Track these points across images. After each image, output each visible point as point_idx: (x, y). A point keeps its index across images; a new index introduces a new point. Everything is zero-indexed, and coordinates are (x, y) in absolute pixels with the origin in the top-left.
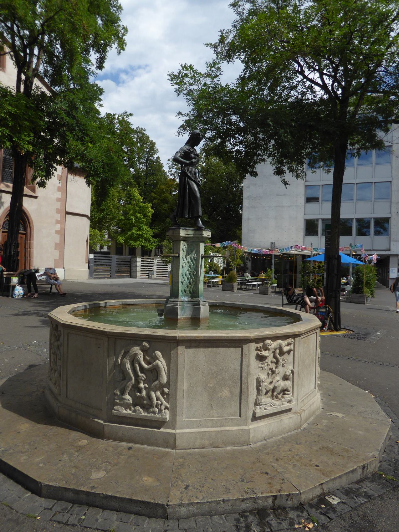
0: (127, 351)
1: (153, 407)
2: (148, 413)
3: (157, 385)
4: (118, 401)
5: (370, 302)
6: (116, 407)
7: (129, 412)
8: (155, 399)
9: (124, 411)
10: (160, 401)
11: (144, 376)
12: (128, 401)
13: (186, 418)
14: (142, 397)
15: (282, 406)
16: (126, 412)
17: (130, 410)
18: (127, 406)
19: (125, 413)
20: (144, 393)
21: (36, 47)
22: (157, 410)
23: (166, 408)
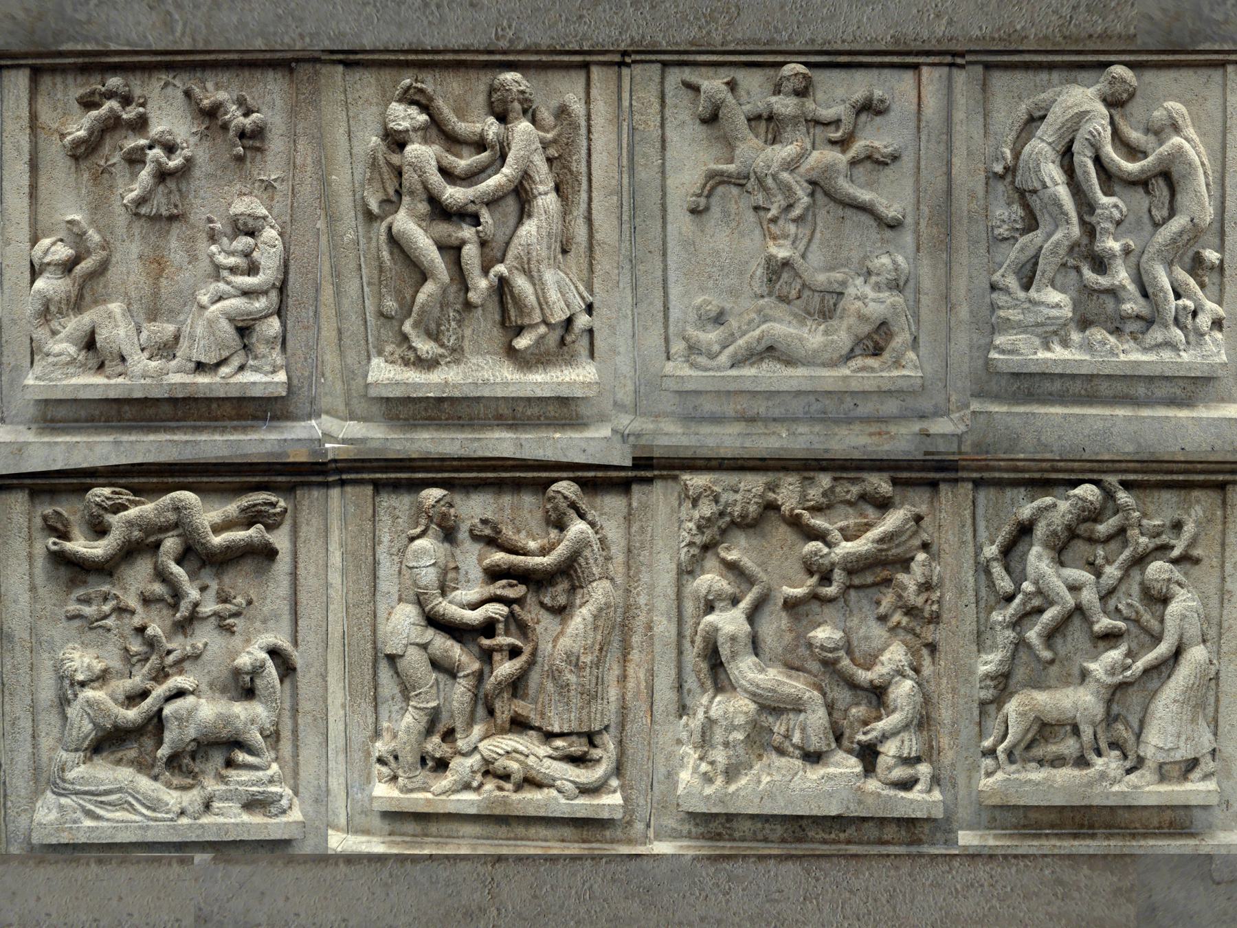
0: (1037, 114)
1: (1166, 326)
2: (1146, 350)
3: (1181, 233)
4: (1014, 315)
5: (784, 614)
6: (999, 340)
7: (1059, 353)
8: (1171, 296)
9: (1042, 355)
10: (1189, 298)
11: (1121, 204)
12: (1054, 313)
13: (351, 828)
14: (1113, 292)
15: (205, 820)
16: (1048, 355)
17: (1065, 343)
18: (1052, 333)
19: (1045, 361)
20: (1122, 276)
21: (811, 634)
22: (1178, 334)
23: (1217, 324)
